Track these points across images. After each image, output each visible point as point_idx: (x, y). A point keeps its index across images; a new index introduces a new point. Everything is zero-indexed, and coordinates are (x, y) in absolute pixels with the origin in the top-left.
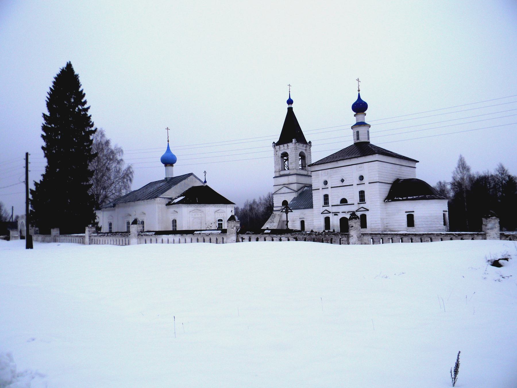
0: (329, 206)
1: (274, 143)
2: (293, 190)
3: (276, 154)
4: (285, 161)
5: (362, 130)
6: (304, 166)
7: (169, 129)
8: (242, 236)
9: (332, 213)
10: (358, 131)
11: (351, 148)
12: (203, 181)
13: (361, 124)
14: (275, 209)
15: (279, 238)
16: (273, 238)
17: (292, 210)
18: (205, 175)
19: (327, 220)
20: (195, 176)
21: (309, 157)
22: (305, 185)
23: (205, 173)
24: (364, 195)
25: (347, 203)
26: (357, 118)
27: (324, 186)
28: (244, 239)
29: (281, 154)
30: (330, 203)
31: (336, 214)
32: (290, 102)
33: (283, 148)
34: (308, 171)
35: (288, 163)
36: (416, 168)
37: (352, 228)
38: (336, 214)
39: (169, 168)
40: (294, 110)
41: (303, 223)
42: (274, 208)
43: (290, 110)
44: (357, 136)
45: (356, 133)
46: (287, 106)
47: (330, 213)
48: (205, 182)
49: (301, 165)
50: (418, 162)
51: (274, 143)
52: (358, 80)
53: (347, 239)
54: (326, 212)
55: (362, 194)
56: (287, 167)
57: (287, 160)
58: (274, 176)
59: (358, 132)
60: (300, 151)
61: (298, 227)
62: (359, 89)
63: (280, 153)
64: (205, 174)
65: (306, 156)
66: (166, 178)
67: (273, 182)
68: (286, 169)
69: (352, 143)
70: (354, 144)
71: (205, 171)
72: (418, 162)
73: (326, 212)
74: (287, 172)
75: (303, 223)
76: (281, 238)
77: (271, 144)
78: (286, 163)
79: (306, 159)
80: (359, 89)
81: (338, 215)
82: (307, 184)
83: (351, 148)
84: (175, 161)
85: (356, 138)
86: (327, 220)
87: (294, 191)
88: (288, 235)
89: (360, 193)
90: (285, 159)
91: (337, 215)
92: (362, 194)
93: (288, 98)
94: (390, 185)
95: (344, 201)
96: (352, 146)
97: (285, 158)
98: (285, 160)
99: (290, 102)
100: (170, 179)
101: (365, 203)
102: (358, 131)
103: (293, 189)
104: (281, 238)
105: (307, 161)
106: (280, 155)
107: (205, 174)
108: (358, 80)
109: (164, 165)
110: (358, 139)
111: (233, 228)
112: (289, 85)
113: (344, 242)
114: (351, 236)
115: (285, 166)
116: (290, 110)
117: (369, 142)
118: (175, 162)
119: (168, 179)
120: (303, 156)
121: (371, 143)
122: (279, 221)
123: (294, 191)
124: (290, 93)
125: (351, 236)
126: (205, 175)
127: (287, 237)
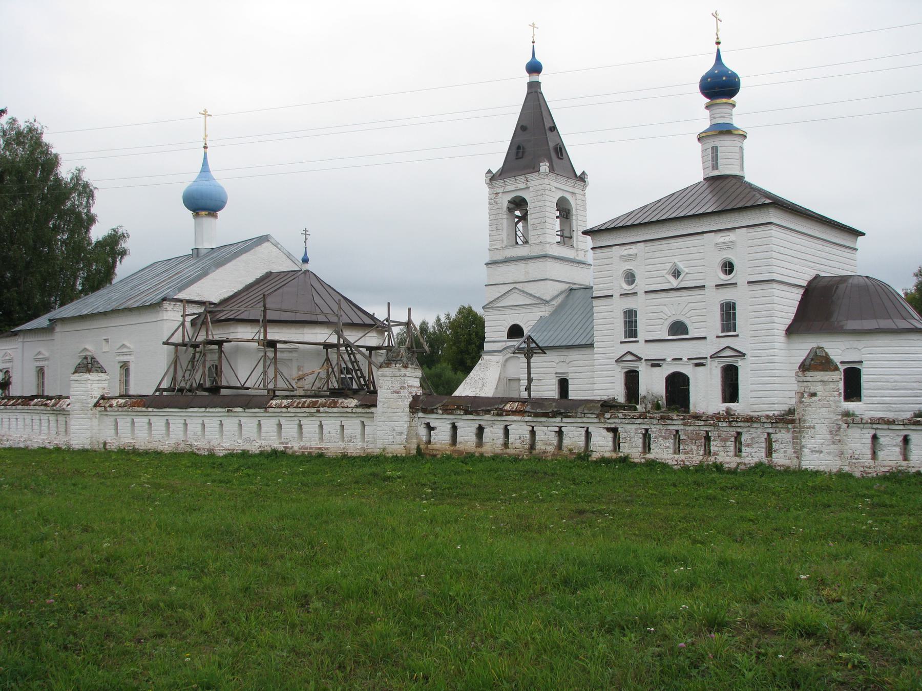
0: (637, 342)
1: (489, 172)
2: (539, 298)
3: (493, 202)
4: (517, 223)
5: (725, 144)
6: (569, 236)
7: (210, 115)
8: (428, 421)
9: (646, 360)
10: (717, 147)
11: (630, 217)
12: (300, 257)
13: (725, 130)
14: (487, 347)
15: (557, 429)
16: (535, 429)
17: (545, 351)
18: (305, 242)
19: (632, 378)
20: (276, 245)
21: (580, 212)
22: (568, 285)
23: (306, 234)
24: (734, 314)
25: (687, 334)
26: (713, 112)
27: (627, 288)
28: (433, 429)
29: (509, 202)
30: (642, 335)
31: (656, 363)
32: (534, 68)
33: (514, 187)
34: (577, 250)
35: (526, 227)
36: (857, 250)
37: (814, 399)
38: (656, 363)
39: (207, 221)
40: (543, 89)
41: (563, 384)
42: (485, 345)
43: (534, 89)
44: (713, 160)
45: (710, 151)
46: (526, 78)
47: (640, 359)
48: (305, 260)
49: (559, 233)
50: (863, 234)
51: (489, 172)
52: (715, 15)
53: (794, 438)
54: (630, 357)
55: (729, 312)
56: (522, 238)
57: (524, 218)
58: (487, 261)
59: (715, 149)
60: (560, 194)
61: (618, 392)
62: (718, 38)
63: (504, 201)
64: (306, 239)
65: (574, 212)
66: (196, 252)
67: (482, 274)
68: (520, 242)
69: (700, 178)
70: (705, 179)
71: (306, 231)
72: (863, 234)
73: (630, 357)
74: (522, 251)
75: (563, 384)
76: (563, 429)
77: (482, 179)
78: (520, 225)
79: (574, 218)
80: (718, 38)
81: (660, 366)
82: (575, 284)
83: (630, 217)
84: (220, 207)
85: (710, 164)
86: (632, 378)
87: (539, 301)
88: (585, 420)
89: (722, 309)
90: (517, 217)
91: (659, 365)
92: (729, 312)
93: (529, 59)
94: (801, 291)
95: (678, 328)
96: (633, 214)
97: (518, 213)
98: (516, 220)
99: (534, 68)
100: (206, 251)
101: (737, 336)
102: (717, 147)
103: (537, 295)
104: (560, 428)
105: (574, 223)
106: (505, 204)
107: (306, 239)
108: (715, 15)
109: (190, 213)
110: (715, 167)
111: (398, 393)
112: (533, 25)
113: (782, 446)
114: (810, 428)
115: (516, 234)
116: (534, 89)
117: (743, 177)
118: (225, 203)
119: (203, 252)
120: (564, 211)
121: (748, 179)
122: (499, 378)
123: (541, 299)
124: (533, 46)
125: (810, 428)
126: (305, 242)
127: (582, 425)
